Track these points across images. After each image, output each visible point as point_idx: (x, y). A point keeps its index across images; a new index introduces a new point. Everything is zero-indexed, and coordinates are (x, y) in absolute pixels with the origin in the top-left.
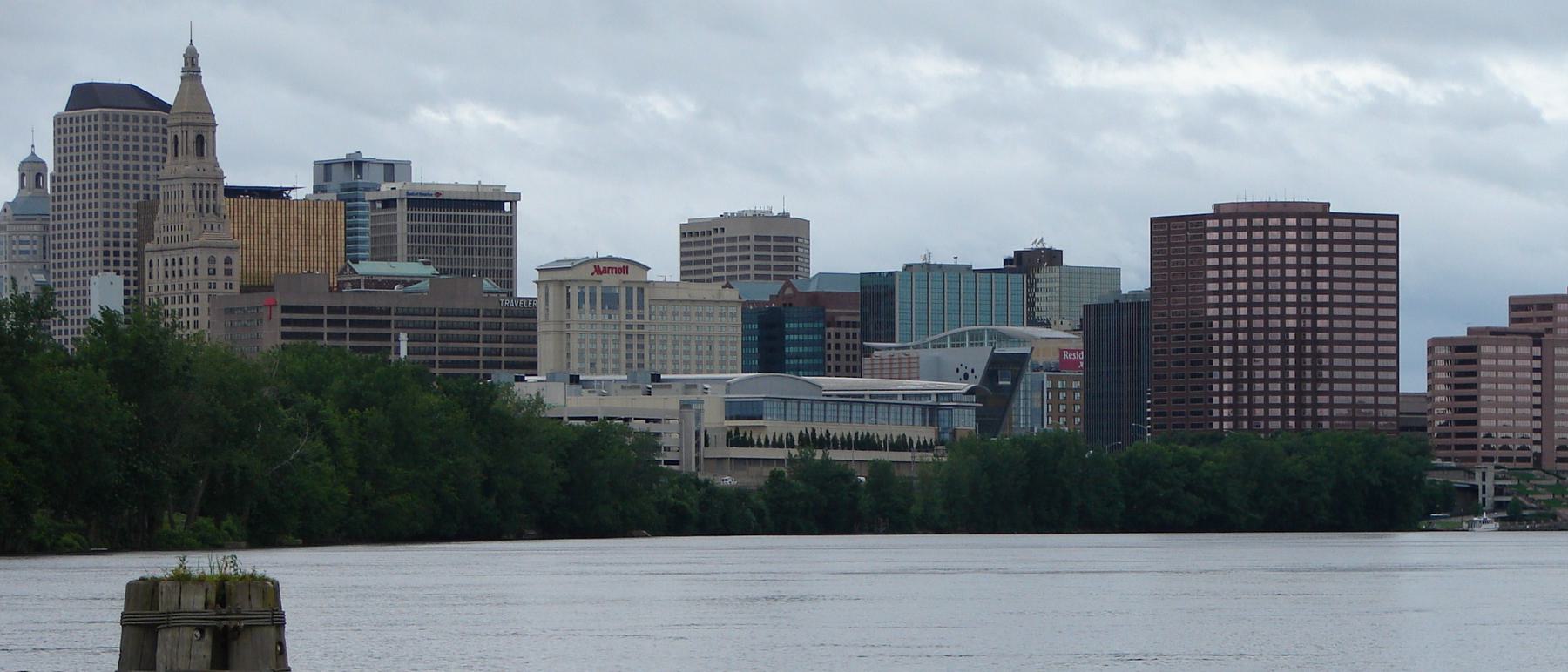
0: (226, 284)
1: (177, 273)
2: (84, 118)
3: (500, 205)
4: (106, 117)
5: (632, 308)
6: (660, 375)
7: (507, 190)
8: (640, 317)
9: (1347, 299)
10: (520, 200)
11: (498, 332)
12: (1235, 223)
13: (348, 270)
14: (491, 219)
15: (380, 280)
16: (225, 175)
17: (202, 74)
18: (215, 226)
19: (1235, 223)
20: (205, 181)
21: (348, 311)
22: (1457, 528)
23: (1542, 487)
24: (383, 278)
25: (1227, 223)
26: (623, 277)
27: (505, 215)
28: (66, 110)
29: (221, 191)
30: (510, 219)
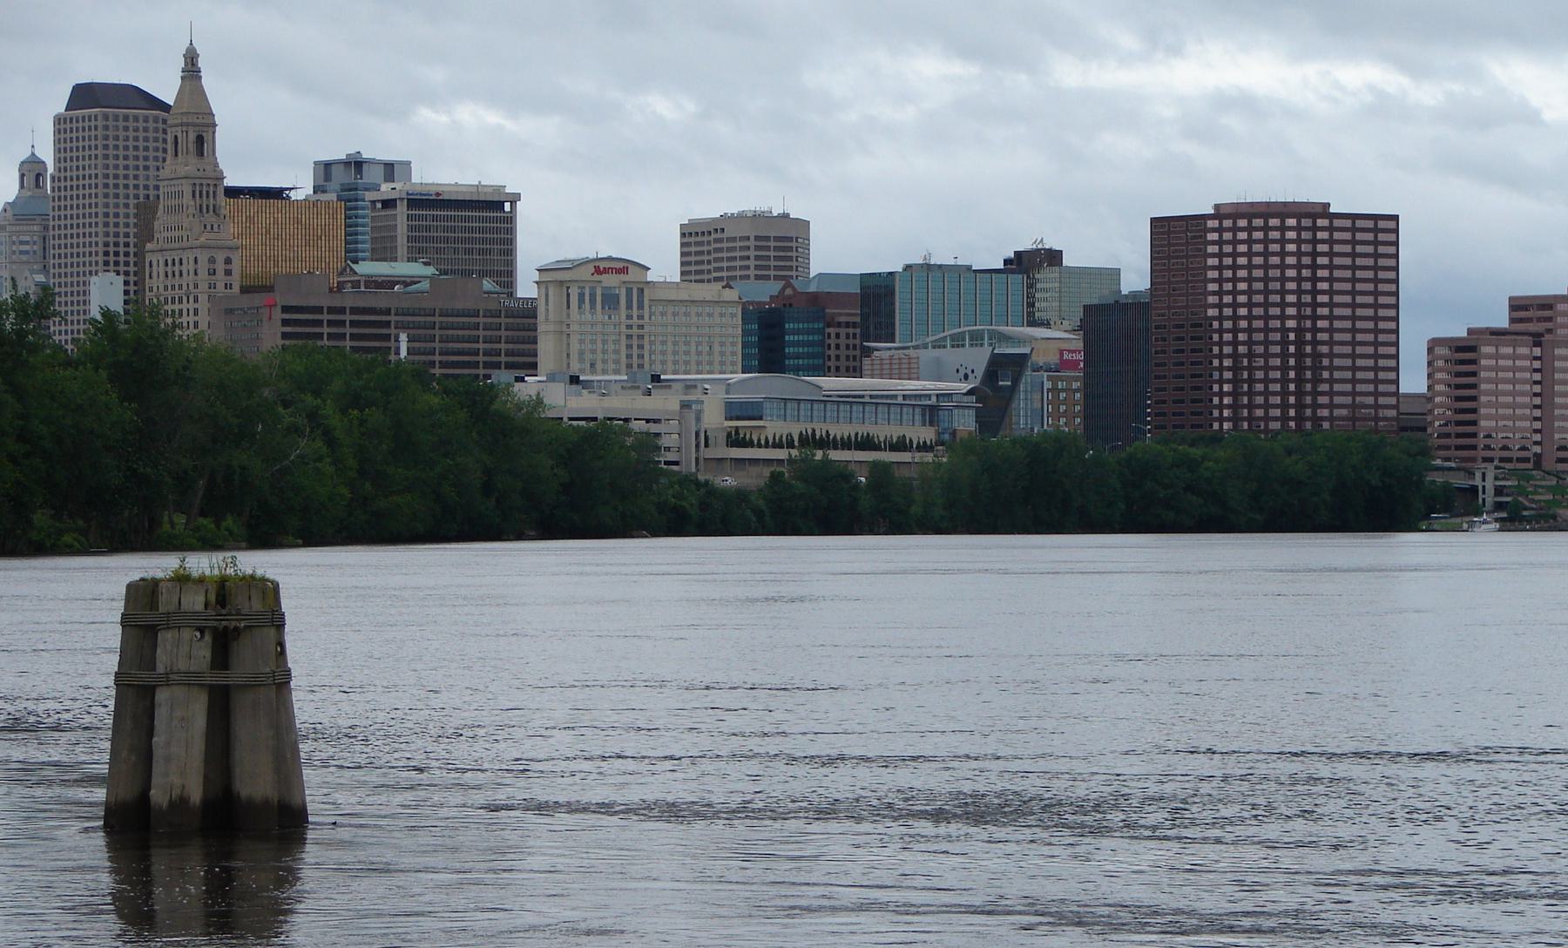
0: (226, 284)
1: (177, 274)
4: (106, 117)
5: (632, 309)
7: (507, 190)
8: (640, 317)
10: (520, 200)
12: (1235, 223)
14: (491, 220)
16: (225, 175)
17: (202, 74)
19: (1235, 223)
23: (1543, 487)
25: (1227, 223)
26: (623, 277)
27: (505, 215)
28: (66, 111)
29: (221, 192)
30: (510, 219)
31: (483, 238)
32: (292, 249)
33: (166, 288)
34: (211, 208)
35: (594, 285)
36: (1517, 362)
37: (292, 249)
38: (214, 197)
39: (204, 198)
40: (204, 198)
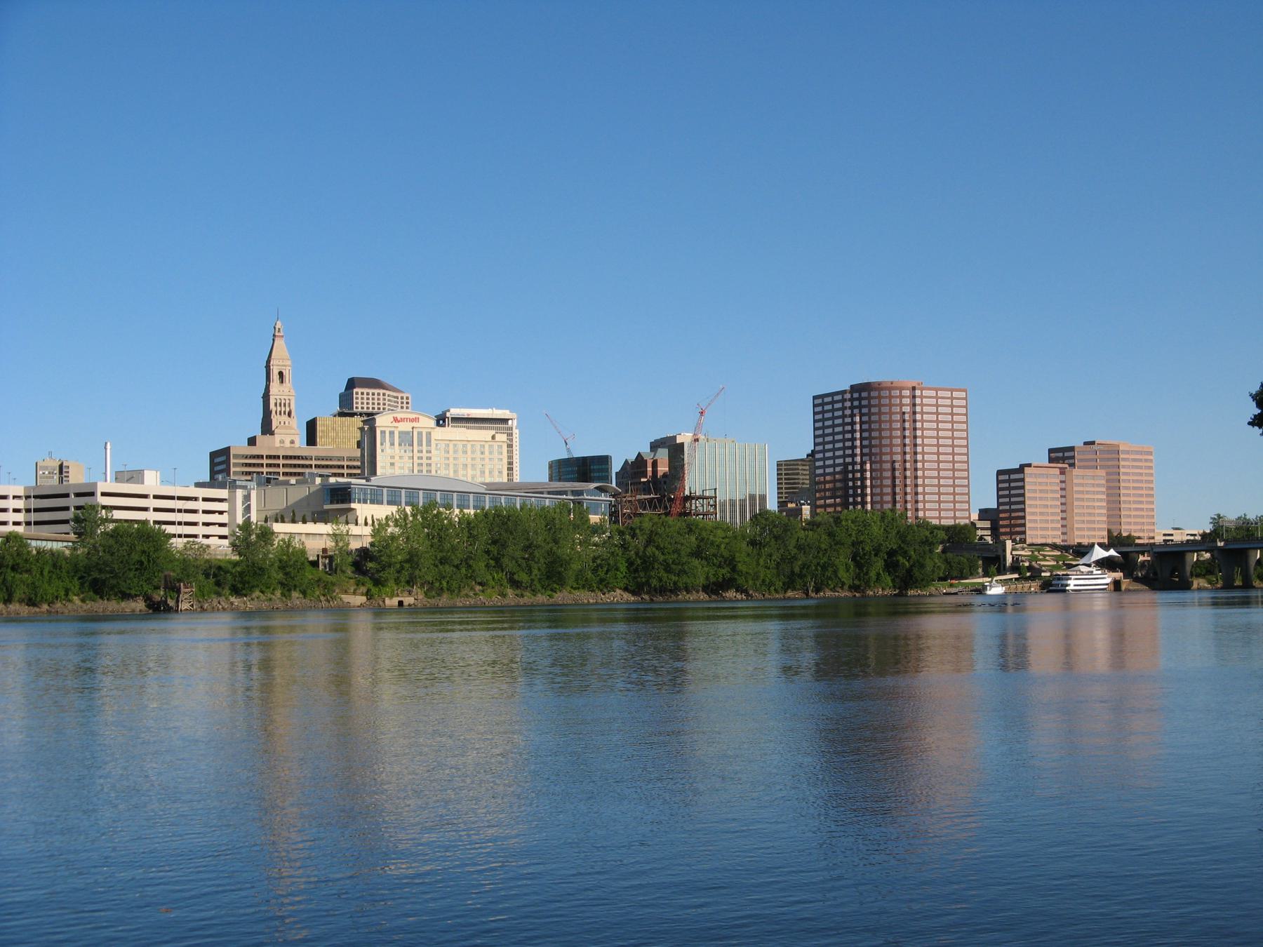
5: (422, 445)
8: (428, 452)
9: (949, 442)
12: (860, 395)
19: (860, 395)
22: (167, 619)
23: (1049, 556)
25: (856, 395)
26: (415, 424)
28: (345, 390)
35: (448, 442)
36: (1007, 478)
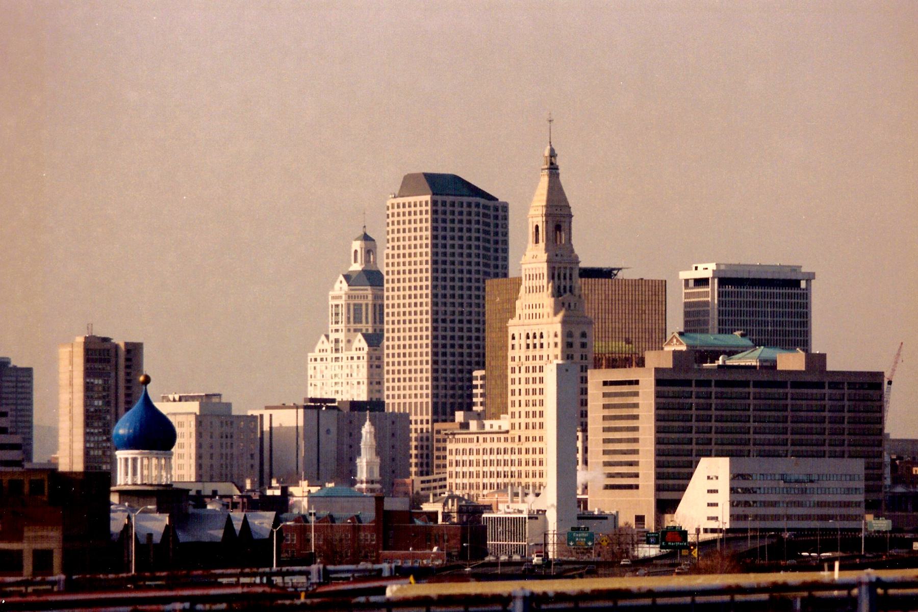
0: (582, 355)
1: (538, 346)
2: (421, 202)
3: (796, 283)
4: (469, 205)
6: (481, 365)
7: (803, 270)
10: (814, 279)
11: (842, 402)
13: (675, 340)
14: (790, 296)
15: (703, 350)
16: (580, 260)
17: (560, 171)
18: (572, 305)
20: (562, 265)
21: (713, 384)
24: (705, 348)
27: (802, 291)
29: (576, 273)
30: (806, 295)
31: (804, 322)
32: (620, 321)
33: (527, 358)
34: (568, 288)
37: (620, 321)
38: (571, 279)
39: (562, 280)
40: (568, 279)
